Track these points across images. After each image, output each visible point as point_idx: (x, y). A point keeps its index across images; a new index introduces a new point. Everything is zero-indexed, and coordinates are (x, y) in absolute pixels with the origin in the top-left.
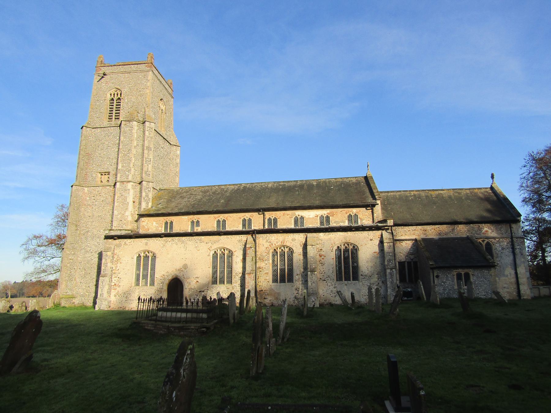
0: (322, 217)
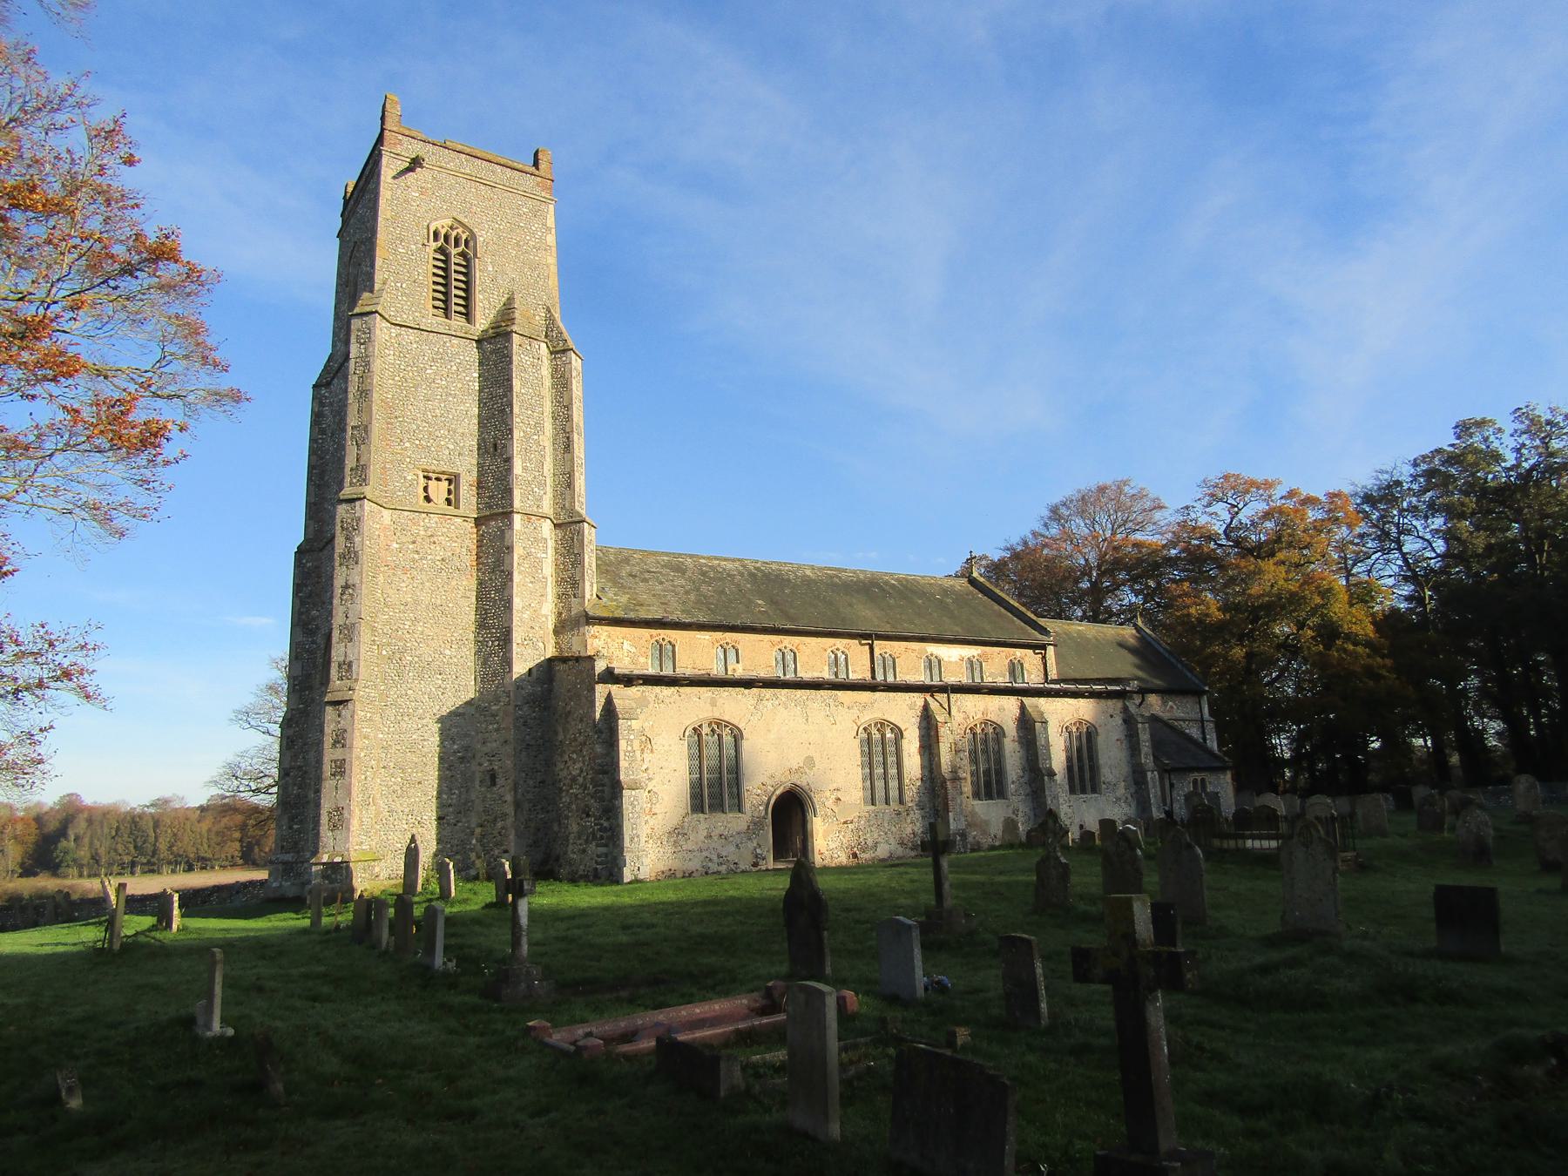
0: (970, 662)
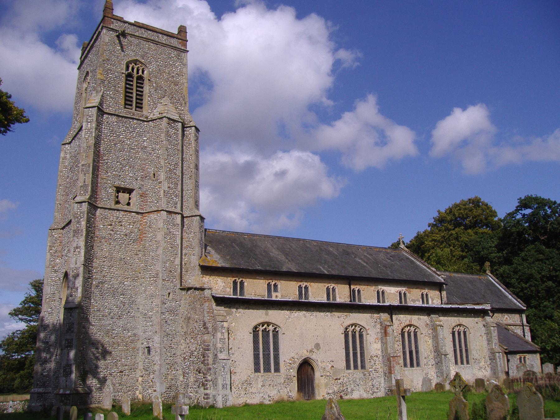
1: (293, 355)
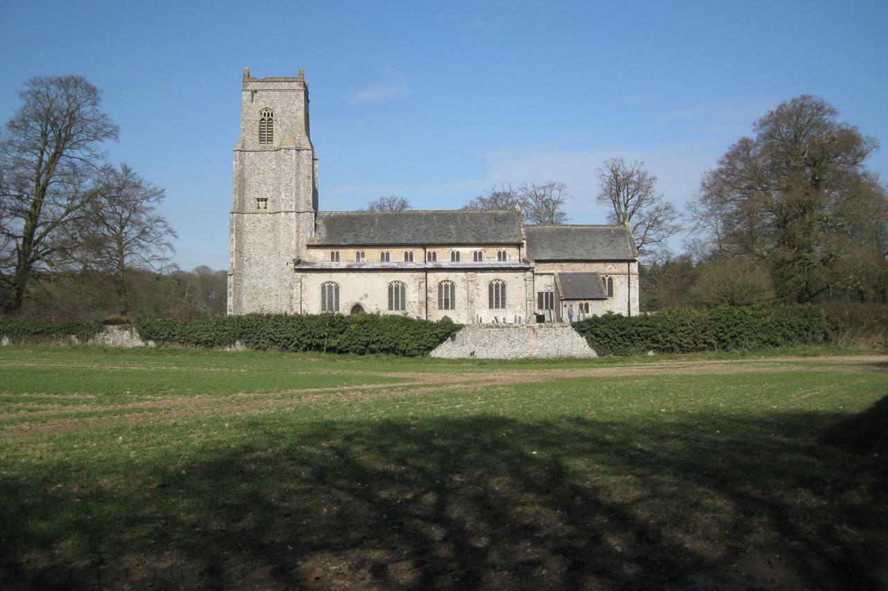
0: (475, 253)
1: (347, 301)
